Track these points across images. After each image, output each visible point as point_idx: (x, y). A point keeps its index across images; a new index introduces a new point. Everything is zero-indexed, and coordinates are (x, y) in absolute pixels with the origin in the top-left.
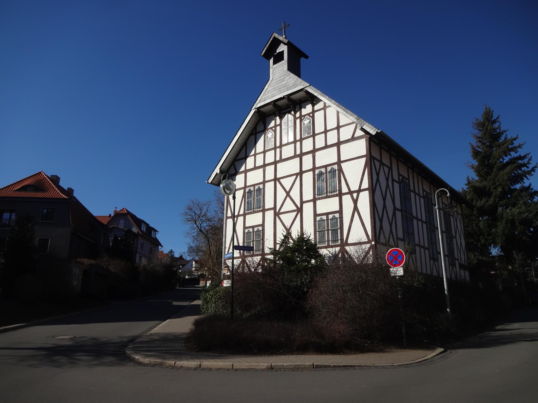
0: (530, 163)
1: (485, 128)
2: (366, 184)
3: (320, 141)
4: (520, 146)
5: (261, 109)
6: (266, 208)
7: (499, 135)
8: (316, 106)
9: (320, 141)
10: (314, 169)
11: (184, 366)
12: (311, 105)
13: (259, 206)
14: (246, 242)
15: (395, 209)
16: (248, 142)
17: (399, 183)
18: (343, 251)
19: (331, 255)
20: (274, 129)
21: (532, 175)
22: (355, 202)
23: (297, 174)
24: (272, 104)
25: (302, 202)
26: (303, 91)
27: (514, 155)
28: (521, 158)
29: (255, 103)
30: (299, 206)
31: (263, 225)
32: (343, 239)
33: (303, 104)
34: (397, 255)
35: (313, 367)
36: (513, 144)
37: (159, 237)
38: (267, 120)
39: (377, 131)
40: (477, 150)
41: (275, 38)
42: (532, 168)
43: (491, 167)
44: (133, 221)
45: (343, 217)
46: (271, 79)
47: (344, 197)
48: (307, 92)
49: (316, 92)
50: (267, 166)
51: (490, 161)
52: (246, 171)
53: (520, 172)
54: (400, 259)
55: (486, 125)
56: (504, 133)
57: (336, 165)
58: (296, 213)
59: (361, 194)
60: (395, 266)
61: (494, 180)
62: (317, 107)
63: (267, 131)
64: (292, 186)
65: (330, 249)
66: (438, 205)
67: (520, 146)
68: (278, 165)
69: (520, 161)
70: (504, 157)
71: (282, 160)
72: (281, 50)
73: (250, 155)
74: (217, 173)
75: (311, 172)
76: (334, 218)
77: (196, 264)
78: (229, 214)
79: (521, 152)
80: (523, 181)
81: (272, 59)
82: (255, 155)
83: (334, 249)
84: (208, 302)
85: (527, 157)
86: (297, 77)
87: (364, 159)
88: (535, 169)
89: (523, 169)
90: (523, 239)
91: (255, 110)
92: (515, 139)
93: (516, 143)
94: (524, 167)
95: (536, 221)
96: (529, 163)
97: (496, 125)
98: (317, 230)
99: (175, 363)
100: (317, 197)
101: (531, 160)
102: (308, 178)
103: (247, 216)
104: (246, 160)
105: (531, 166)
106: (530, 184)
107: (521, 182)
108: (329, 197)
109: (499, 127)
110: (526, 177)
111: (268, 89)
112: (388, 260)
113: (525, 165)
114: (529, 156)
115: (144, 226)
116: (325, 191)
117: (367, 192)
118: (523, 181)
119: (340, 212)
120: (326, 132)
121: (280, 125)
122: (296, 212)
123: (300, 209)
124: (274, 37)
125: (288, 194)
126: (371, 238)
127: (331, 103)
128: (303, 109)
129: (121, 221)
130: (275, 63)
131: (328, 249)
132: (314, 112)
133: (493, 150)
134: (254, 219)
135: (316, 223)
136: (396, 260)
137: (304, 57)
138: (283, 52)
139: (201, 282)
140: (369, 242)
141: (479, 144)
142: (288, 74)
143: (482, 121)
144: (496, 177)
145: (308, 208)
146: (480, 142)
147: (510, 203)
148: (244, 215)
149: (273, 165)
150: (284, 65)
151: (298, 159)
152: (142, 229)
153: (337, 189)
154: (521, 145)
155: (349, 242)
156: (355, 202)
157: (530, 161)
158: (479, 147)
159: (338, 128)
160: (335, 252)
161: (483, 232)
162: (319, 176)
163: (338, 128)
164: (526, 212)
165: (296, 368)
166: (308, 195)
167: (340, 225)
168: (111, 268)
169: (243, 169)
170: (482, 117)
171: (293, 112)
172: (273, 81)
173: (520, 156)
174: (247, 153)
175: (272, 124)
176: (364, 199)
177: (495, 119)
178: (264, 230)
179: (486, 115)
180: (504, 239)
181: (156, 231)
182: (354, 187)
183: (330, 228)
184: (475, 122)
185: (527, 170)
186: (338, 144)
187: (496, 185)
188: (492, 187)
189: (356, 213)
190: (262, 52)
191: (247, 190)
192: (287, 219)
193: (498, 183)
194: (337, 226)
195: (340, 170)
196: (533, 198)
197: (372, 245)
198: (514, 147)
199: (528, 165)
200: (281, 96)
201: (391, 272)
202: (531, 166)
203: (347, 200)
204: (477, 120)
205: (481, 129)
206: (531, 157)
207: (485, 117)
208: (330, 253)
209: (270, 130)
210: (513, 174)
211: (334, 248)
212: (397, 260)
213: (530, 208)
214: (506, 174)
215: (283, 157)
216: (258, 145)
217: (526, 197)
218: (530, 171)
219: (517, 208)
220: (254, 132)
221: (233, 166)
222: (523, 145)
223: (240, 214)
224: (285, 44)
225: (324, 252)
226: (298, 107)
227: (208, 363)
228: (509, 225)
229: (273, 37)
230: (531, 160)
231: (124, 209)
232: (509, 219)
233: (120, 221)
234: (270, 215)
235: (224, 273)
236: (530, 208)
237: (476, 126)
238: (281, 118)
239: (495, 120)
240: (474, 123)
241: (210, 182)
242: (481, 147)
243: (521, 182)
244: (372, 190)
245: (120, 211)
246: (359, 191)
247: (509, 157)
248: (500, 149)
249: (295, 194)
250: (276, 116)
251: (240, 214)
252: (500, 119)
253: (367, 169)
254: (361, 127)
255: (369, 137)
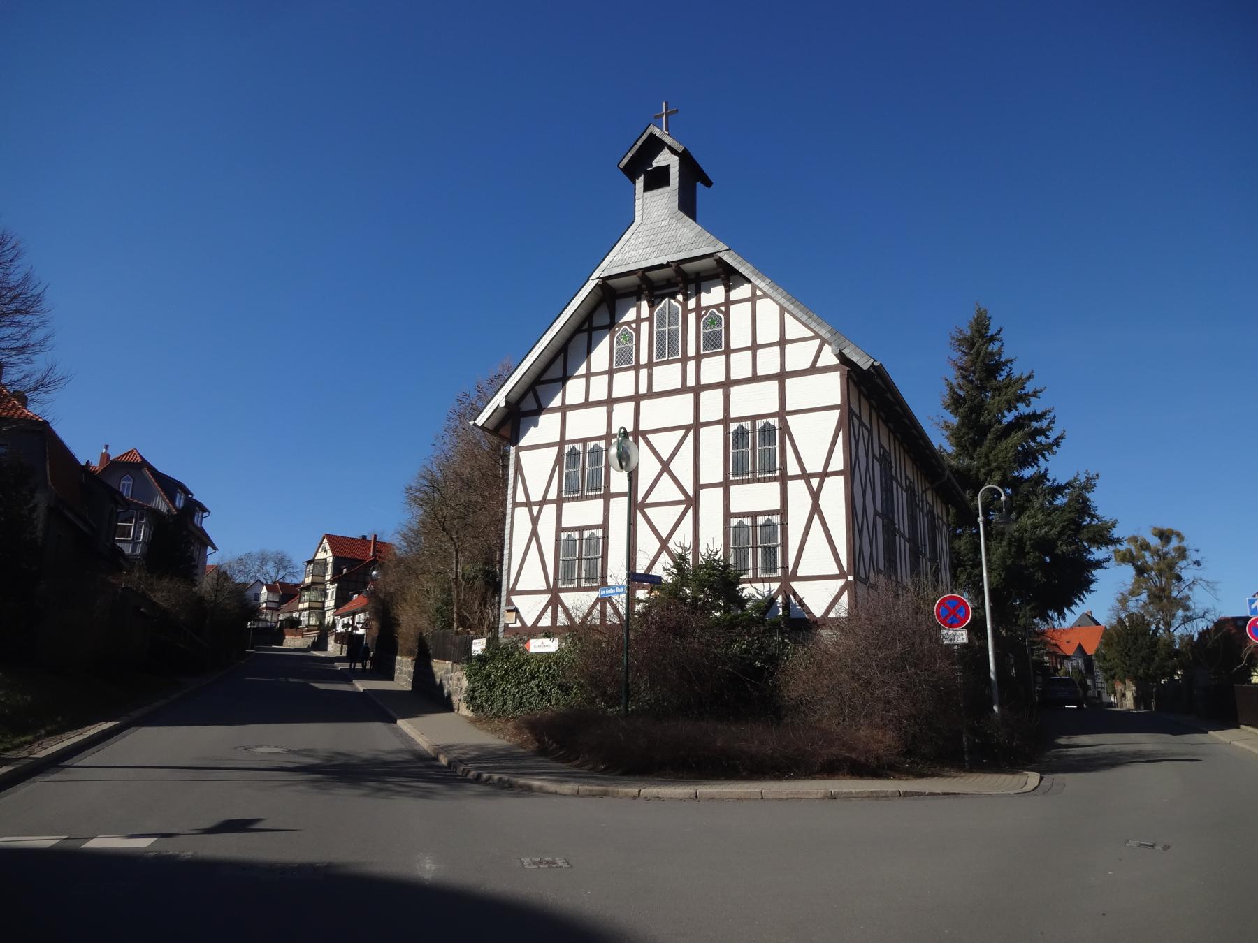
0: (1051, 429)
1: (975, 350)
2: (838, 463)
3: (741, 366)
4: (1035, 394)
5: (610, 282)
6: (611, 492)
7: (998, 367)
8: (733, 291)
9: (741, 366)
10: (726, 421)
11: (660, 796)
12: (723, 286)
13: (595, 485)
14: (564, 560)
15: (876, 513)
16: (570, 345)
17: (880, 461)
18: (787, 591)
19: (760, 597)
20: (723, 309)
21: (1054, 453)
22: (815, 495)
23: (687, 428)
24: (640, 274)
25: (698, 487)
26: (712, 258)
27: (1023, 409)
28: (1036, 417)
29: (598, 266)
30: (691, 493)
31: (605, 527)
32: (787, 567)
33: (703, 284)
34: (955, 607)
35: (899, 794)
36: (1023, 389)
37: (209, 525)
38: (616, 304)
39: (873, 363)
40: (956, 393)
41: (652, 136)
42: (1055, 439)
43: (983, 430)
44: (156, 484)
45: (787, 524)
46: (638, 220)
47: (790, 484)
48: (721, 262)
49: (747, 269)
50: (615, 403)
51: (982, 419)
52: (564, 409)
53: (1033, 444)
54: (962, 614)
55: (977, 345)
56: (1009, 364)
57: (777, 419)
58: (682, 507)
59: (828, 480)
60: (951, 626)
61: (987, 457)
62: (735, 295)
63: (617, 329)
64: (674, 450)
65: (759, 586)
66: (983, 516)
67: (1035, 394)
68: (643, 404)
69: (1034, 424)
70: (1006, 413)
71: (651, 395)
72: (663, 164)
73: (576, 374)
74: (498, 405)
75: (720, 428)
76: (768, 524)
77: (271, 595)
78: (521, 497)
79: (1037, 406)
80: (1037, 464)
81: (642, 178)
82: (588, 376)
83: (767, 585)
84: (494, 685)
85: (1047, 417)
86: (691, 221)
87: (837, 413)
88: (1060, 441)
89: (1039, 439)
90: (1036, 578)
91: (598, 280)
92: (1029, 378)
93: (1029, 388)
94: (1040, 435)
95: (1061, 545)
96: (1049, 428)
97: (994, 347)
98: (732, 546)
99: (640, 791)
100: (564, 496)
101: (1054, 423)
102: (712, 439)
103: (532, 500)
104: (564, 384)
105: (1053, 435)
106: (1046, 470)
107: (1033, 464)
108: (759, 481)
109: (999, 353)
110: (1043, 455)
111: (630, 241)
112: (939, 617)
113: (1042, 432)
114: (1051, 415)
115: (180, 499)
116: (750, 468)
117: (840, 480)
118: (1037, 464)
119: (783, 511)
120: (754, 347)
121: (650, 319)
122: (684, 506)
123: (694, 500)
124: (651, 133)
125: (665, 466)
126: (846, 569)
127: (779, 295)
128: (703, 295)
129: (124, 482)
130: (648, 187)
131: (753, 585)
132: (728, 303)
133: (987, 396)
134: (583, 513)
135: (728, 531)
136: (954, 616)
137: (701, 183)
138: (668, 167)
139: (287, 637)
140: (842, 575)
141: (961, 381)
142: (679, 217)
143: (969, 334)
144: (991, 452)
145: (711, 501)
146: (964, 377)
147: (1014, 505)
148: (559, 502)
149: (632, 401)
150: (667, 197)
151: (691, 396)
152: (177, 503)
153: (778, 466)
154: (1037, 392)
155: (800, 573)
156: (815, 495)
157: (1052, 425)
158: (961, 388)
159: (782, 343)
160: (770, 591)
161: (965, 559)
162: (737, 437)
163: (782, 343)
164: (1046, 525)
165: (875, 796)
166: (712, 470)
167: (782, 539)
168: (159, 597)
169: (556, 402)
170: (969, 326)
171: (680, 297)
172: (642, 227)
173: (1035, 413)
174: (568, 369)
175: (631, 315)
176: (834, 495)
177: (994, 333)
178: (608, 537)
179: (978, 324)
180: (1002, 577)
181: (204, 510)
182: (815, 466)
183: (759, 544)
184: (954, 335)
185: (1046, 442)
186: (782, 377)
187: (991, 467)
188: (983, 470)
189: (816, 517)
190: (621, 161)
191: (567, 448)
192: (664, 518)
193: (994, 464)
194: (777, 542)
195: (785, 429)
196: (1054, 497)
197: (847, 582)
198: (1025, 394)
199: (1047, 433)
200: (663, 260)
201: (944, 637)
202: (1053, 435)
203: (798, 490)
204: (960, 332)
205: (966, 351)
206: (1055, 417)
207: (975, 328)
208: (758, 593)
209: (624, 327)
210: (1019, 448)
211: (768, 584)
212: (955, 615)
213: (1051, 518)
214: (1012, 447)
215: (655, 389)
216: (594, 355)
217: (1045, 495)
218: (1050, 444)
219: (1028, 516)
220: (586, 326)
221: (531, 394)
222: (1041, 391)
223: (549, 498)
224: (673, 151)
225: (748, 590)
226: (692, 287)
227: (704, 790)
228: (1014, 549)
229: (648, 132)
230: (1054, 423)
231: (133, 451)
232: (1013, 536)
233: (122, 482)
234: (620, 507)
235: (505, 624)
236: (1051, 518)
237: (957, 343)
238: (652, 306)
239: (992, 336)
240: (953, 338)
241: (480, 425)
242: (965, 388)
243: (1033, 464)
244: (850, 473)
245: (123, 456)
246: (824, 474)
247: (1015, 413)
248: (999, 395)
249: (682, 466)
250: (639, 299)
251: (549, 498)
252: (1001, 336)
253: (841, 432)
254: (840, 351)
255: (848, 370)
